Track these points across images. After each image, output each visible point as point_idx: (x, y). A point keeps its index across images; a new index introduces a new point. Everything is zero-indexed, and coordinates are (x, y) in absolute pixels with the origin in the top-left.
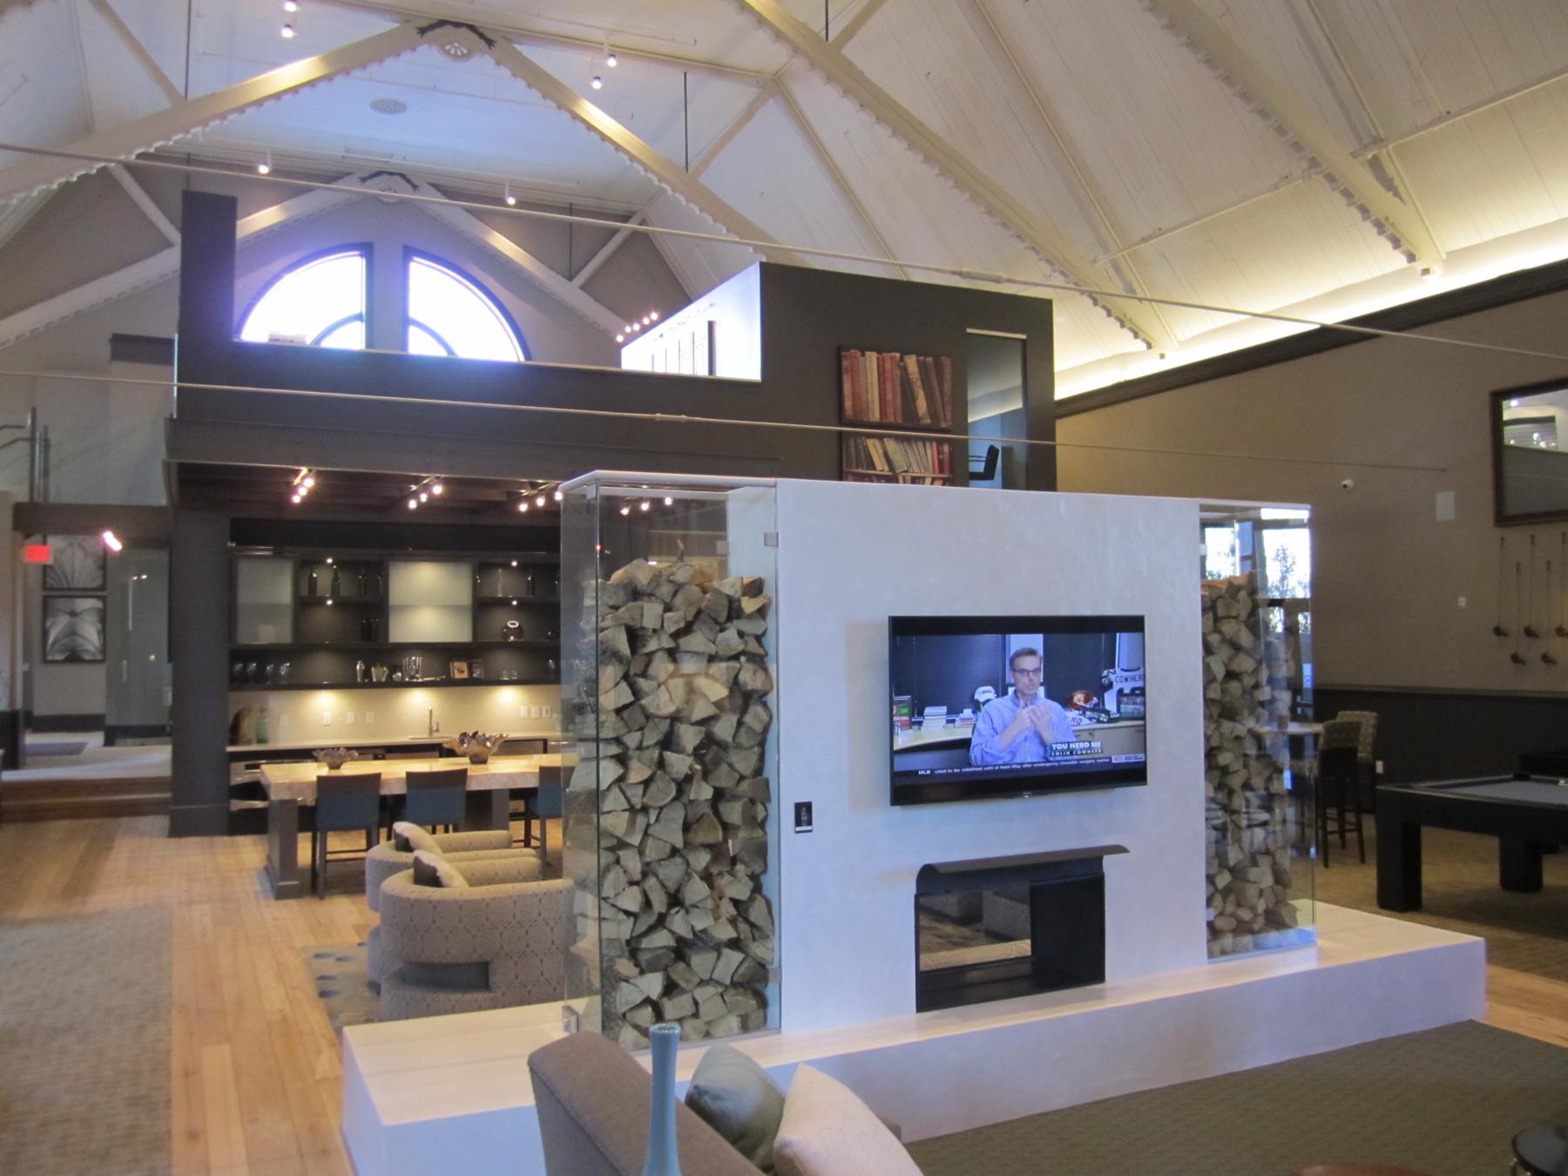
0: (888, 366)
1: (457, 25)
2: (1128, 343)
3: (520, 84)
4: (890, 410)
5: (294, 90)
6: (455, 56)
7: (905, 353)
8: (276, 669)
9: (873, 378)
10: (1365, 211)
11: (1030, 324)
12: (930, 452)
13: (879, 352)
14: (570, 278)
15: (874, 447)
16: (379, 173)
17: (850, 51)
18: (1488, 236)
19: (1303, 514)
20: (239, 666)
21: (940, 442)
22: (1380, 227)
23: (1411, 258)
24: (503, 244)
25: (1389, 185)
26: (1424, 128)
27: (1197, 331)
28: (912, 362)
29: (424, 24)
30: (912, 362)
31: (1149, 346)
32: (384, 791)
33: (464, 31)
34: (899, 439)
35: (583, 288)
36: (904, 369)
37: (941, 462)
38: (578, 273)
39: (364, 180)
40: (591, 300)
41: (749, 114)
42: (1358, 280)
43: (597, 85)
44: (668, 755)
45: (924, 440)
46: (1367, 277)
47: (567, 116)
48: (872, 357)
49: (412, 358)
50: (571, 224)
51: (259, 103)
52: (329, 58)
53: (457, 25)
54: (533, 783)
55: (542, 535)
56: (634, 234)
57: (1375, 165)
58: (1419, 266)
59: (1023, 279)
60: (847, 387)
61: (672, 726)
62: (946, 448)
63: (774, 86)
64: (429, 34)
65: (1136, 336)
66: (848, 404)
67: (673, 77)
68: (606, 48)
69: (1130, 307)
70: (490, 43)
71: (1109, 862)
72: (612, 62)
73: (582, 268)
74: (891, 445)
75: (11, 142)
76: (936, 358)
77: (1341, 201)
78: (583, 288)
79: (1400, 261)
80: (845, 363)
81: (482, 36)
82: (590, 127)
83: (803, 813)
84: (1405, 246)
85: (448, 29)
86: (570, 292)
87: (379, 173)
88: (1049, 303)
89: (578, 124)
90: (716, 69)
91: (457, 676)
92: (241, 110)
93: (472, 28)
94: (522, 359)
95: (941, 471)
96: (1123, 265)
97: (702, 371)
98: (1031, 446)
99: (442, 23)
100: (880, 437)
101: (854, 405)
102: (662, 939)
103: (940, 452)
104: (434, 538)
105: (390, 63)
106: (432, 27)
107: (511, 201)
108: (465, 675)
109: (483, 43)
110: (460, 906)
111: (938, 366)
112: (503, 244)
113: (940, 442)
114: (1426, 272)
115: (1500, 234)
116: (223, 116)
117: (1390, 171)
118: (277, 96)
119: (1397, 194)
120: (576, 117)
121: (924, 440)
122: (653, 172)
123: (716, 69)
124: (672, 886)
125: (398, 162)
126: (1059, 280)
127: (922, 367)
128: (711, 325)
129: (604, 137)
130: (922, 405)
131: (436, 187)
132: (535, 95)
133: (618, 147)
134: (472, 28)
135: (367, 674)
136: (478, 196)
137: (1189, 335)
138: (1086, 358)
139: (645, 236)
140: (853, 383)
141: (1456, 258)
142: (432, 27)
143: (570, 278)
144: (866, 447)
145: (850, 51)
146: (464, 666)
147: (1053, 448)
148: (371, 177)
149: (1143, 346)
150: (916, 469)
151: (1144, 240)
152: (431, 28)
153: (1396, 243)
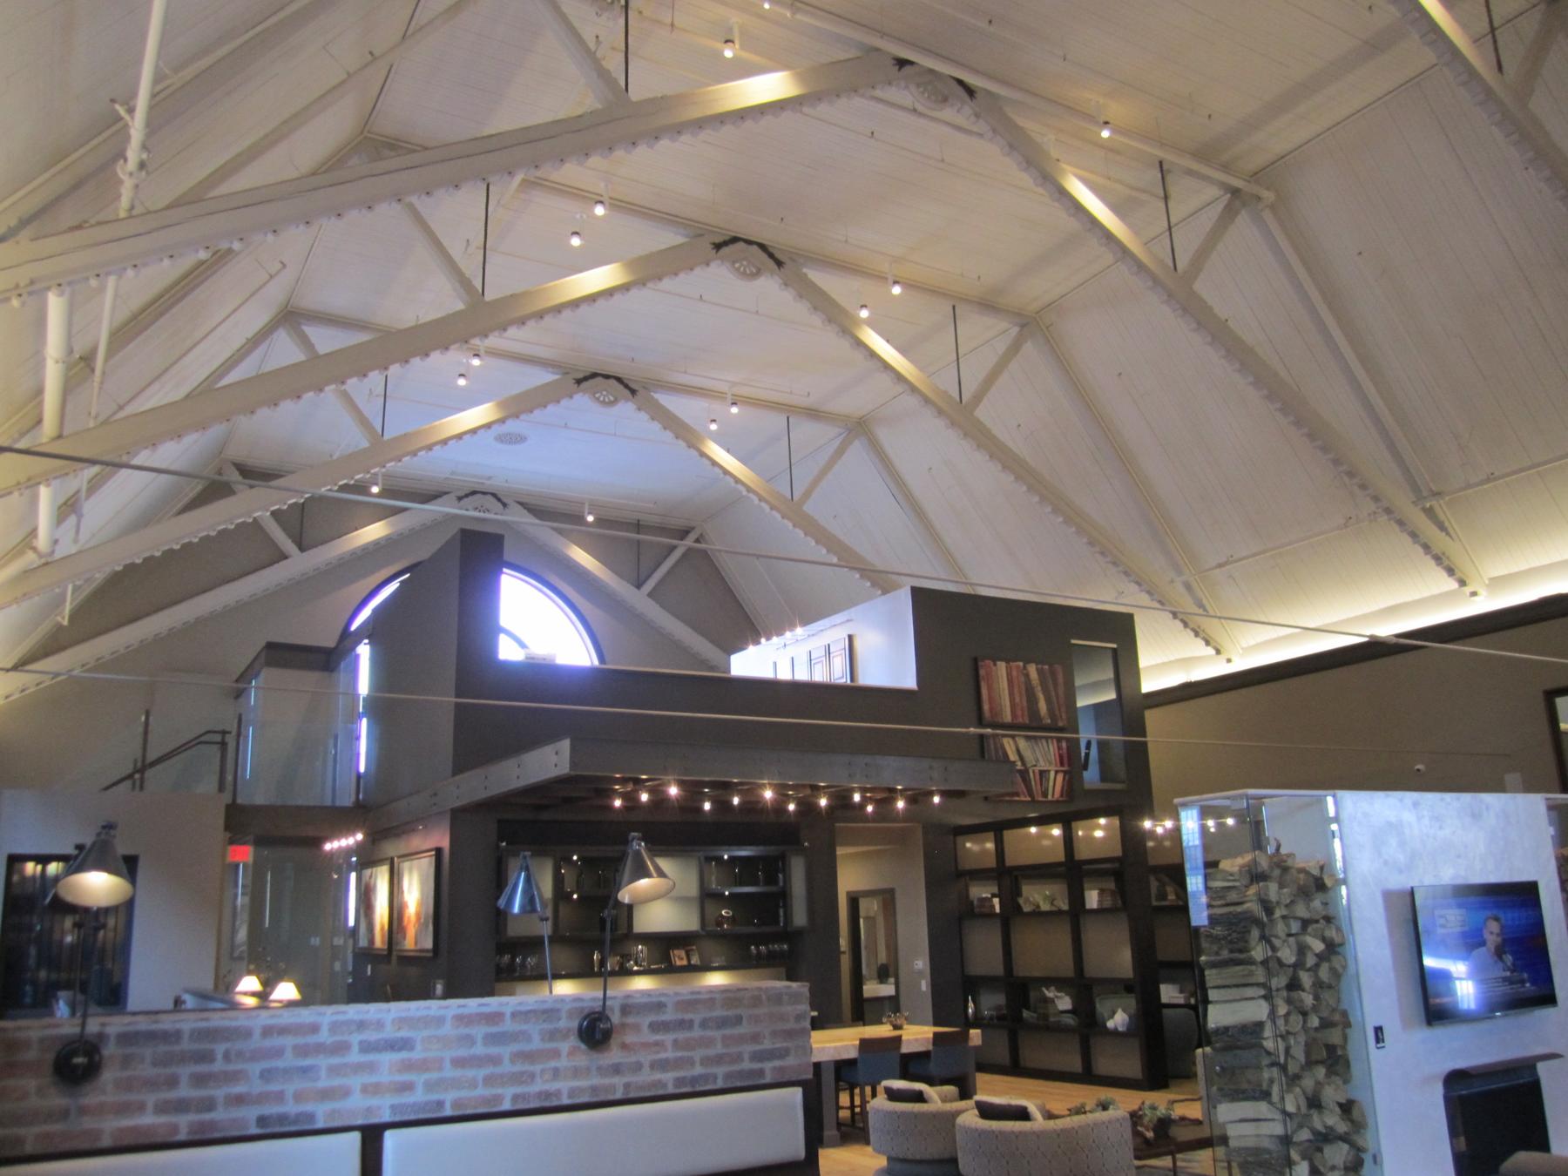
0: (1014, 673)
1: (607, 377)
2: (1199, 649)
3: (656, 426)
4: (1019, 713)
5: (474, 431)
6: (603, 402)
7: (1027, 661)
8: (524, 960)
9: (1004, 684)
10: (1427, 548)
11: (1117, 631)
12: (1052, 748)
13: (1007, 661)
14: (639, 586)
15: (1009, 746)
16: (474, 493)
17: (982, 413)
18: (1523, 566)
19: (1330, 800)
20: (507, 958)
21: (1059, 740)
22: (1438, 559)
23: (1462, 583)
24: (582, 557)
25: (1442, 527)
26: (1477, 485)
27: (1259, 640)
28: (1032, 669)
29: (581, 376)
30: (1032, 669)
31: (1218, 652)
32: (905, 1049)
33: (613, 382)
34: (1028, 738)
35: (650, 595)
36: (1027, 676)
37: (1061, 757)
38: (644, 582)
39: (460, 499)
40: (657, 607)
41: (840, 452)
42: (1409, 599)
43: (713, 427)
44: (1295, 995)
45: (1047, 738)
46: (1417, 596)
47: (695, 453)
48: (1002, 665)
49: (505, 662)
50: (638, 542)
51: (445, 442)
52: (503, 404)
53: (607, 377)
54: (853, 1054)
55: (754, 825)
56: (689, 550)
57: (1430, 513)
58: (1468, 590)
59: (1100, 593)
60: (984, 692)
61: (1295, 972)
62: (1064, 745)
63: (859, 428)
64: (585, 385)
65: (1208, 643)
66: (986, 707)
67: (778, 421)
68: (729, 397)
69: (1205, 623)
70: (633, 392)
71: (1542, 1068)
72: (734, 410)
73: (649, 577)
74: (1022, 743)
75: (173, 468)
76: (1051, 665)
77: (1407, 539)
78: (650, 595)
79: (1452, 585)
80: (982, 672)
81: (627, 386)
82: (714, 463)
83: (1378, 1030)
84: (1459, 574)
85: (599, 379)
86: (639, 600)
87: (474, 493)
88: (1130, 617)
89: (705, 461)
90: (813, 414)
91: (678, 963)
92: (429, 448)
93: (619, 380)
94: (596, 663)
95: (1062, 764)
96: (1194, 585)
97: (845, 680)
98: (457, 705)
99: (594, 375)
100: (1013, 737)
101: (991, 709)
102: (1304, 1135)
103: (1059, 748)
104: (674, 832)
105: (551, 408)
106: (586, 379)
107: (590, 518)
108: (685, 962)
109: (627, 392)
110: (1039, 1135)
111: (1053, 673)
112: (582, 557)
113: (1059, 740)
114: (1474, 594)
115: (1533, 565)
116: (414, 454)
117: (1442, 517)
118: (459, 437)
119: (1448, 534)
120: (703, 455)
121: (1047, 738)
122: (767, 502)
123: (813, 414)
124: (1309, 1090)
125: (491, 485)
126: (1144, 599)
127: (1040, 672)
128: (850, 638)
129: (726, 472)
130: (1043, 706)
131: (521, 504)
132: (668, 435)
133: (737, 480)
134: (619, 380)
135: (602, 963)
136: (559, 514)
137: (1252, 642)
138: (1167, 660)
139: (704, 553)
140: (990, 689)
141: (1497, 583)
142: (586, 379)
143: (639, 586)
144: (1002, 746)
145: (982, 413)
146: (682, 953)
147: (1145, 744)
148: (467, 496)
149: (1213, 652)
150: (1042, 762)
151: (1220, 566)
152: (585, 378)
153: (1451, 571)
